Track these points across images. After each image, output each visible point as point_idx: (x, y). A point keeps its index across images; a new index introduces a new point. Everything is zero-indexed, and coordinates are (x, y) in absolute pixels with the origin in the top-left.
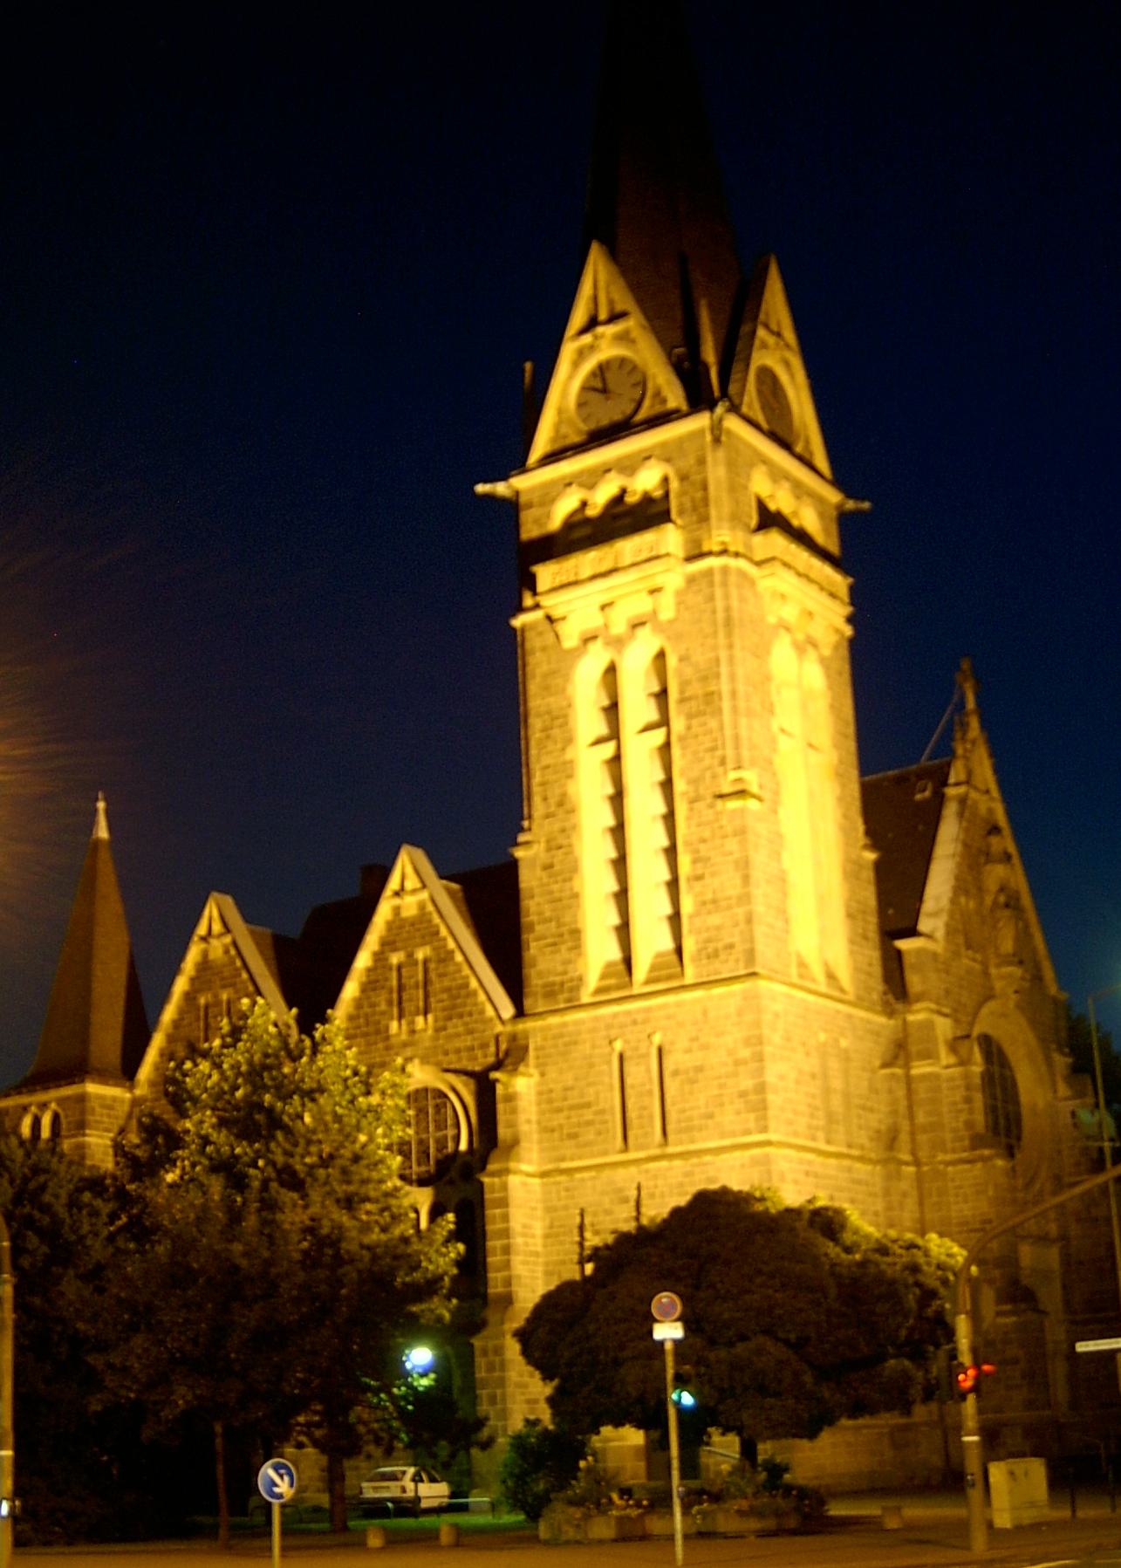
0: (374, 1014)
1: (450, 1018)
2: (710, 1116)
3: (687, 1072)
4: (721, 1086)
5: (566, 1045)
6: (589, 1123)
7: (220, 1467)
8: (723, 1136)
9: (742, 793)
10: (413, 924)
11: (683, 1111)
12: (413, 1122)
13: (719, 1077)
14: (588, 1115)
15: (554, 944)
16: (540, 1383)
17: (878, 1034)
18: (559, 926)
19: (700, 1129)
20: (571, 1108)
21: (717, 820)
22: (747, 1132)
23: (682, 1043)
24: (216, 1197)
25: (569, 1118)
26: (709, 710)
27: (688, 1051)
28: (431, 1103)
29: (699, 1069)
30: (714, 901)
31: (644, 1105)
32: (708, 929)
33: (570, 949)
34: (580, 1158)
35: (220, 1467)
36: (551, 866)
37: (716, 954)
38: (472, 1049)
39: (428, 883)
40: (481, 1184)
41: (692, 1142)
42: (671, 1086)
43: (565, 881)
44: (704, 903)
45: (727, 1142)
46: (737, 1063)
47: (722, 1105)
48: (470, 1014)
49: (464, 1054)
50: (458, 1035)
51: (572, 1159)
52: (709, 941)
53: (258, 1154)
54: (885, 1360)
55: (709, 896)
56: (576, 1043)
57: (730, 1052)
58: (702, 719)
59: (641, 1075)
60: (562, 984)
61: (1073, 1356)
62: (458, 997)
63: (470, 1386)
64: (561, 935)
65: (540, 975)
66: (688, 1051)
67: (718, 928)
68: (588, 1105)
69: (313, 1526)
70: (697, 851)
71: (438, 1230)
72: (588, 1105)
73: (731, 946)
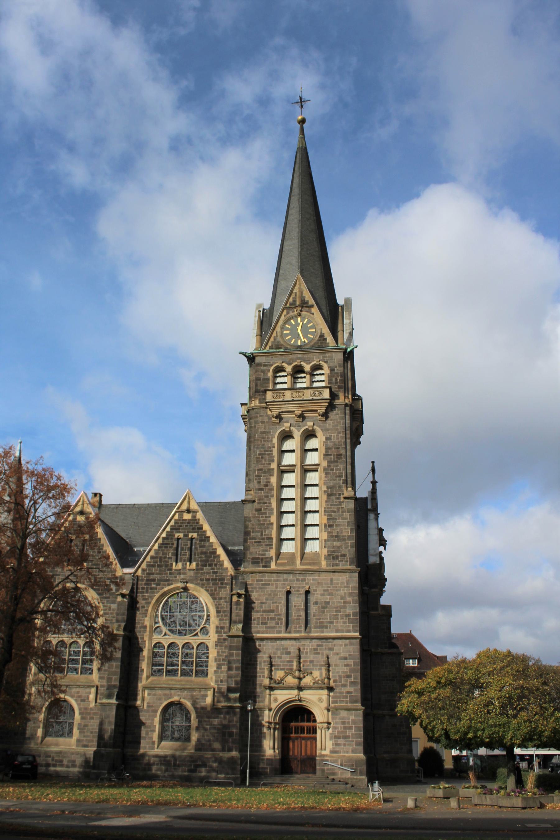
0: (165, 558)
1: (205, 566)
2: (331, 623)
3: (322, 603)
4: (337, 611)
5: (263, 584)
6: (272, 619)
7: (248, 770)
8: (337, 631)
9: (467, 808)
10: (189, 523)
11: (319, 619)
12: (23, 472)
13: (337, 607)
14: (272, 615)
15: (260, 542)
16: (465, 656)
17: (33, 707)
18: (262, 535)
19: (326, 627)
20: (264, 611)
21: (341, 505)
22: (349, 631)
23: (320, 590)
24: (32, 664)
25: (262, 615)
26: (79, 702)
27: (322, 595)
28: (198, 614)
29: (328, 603)
30: (337, 536)
31: (297, 611)
32: (334, 547)
33: (266, 545)
34: (267, 633)
35: (248, 770)
36: (260, 510)
37: (337, 557)
38: (216, 580)
39: (376, 532)
40: (365, 753)
41: (323, 632)
42: (313, 609)
43: (266, 517)
44: (332, 536)
45: (339, 634)
46: (345, 602)
47: (337, 619)
48: (216, 565)
49: (211, 582)
50: (208, 573)
51: (263, 633)
52: (334, 551)
53: (473, 709)
54: (519, 767)
55: (335, 534)
56: (268, 584)
57: (342, 598)
58: (336, 464)
59: (297, 600)
60: (262, 559)
61: (312, 322)
62: (210, 557)
63: (262, 513)
64: (263, 539)
65: (251, 553)
66: (322, 595)
67: (339, 547)
68: (272, 611)
69: (311, 829)
70: (331, 515)
71: (66, 635)
72: (272, 611)
73: (344, 555)
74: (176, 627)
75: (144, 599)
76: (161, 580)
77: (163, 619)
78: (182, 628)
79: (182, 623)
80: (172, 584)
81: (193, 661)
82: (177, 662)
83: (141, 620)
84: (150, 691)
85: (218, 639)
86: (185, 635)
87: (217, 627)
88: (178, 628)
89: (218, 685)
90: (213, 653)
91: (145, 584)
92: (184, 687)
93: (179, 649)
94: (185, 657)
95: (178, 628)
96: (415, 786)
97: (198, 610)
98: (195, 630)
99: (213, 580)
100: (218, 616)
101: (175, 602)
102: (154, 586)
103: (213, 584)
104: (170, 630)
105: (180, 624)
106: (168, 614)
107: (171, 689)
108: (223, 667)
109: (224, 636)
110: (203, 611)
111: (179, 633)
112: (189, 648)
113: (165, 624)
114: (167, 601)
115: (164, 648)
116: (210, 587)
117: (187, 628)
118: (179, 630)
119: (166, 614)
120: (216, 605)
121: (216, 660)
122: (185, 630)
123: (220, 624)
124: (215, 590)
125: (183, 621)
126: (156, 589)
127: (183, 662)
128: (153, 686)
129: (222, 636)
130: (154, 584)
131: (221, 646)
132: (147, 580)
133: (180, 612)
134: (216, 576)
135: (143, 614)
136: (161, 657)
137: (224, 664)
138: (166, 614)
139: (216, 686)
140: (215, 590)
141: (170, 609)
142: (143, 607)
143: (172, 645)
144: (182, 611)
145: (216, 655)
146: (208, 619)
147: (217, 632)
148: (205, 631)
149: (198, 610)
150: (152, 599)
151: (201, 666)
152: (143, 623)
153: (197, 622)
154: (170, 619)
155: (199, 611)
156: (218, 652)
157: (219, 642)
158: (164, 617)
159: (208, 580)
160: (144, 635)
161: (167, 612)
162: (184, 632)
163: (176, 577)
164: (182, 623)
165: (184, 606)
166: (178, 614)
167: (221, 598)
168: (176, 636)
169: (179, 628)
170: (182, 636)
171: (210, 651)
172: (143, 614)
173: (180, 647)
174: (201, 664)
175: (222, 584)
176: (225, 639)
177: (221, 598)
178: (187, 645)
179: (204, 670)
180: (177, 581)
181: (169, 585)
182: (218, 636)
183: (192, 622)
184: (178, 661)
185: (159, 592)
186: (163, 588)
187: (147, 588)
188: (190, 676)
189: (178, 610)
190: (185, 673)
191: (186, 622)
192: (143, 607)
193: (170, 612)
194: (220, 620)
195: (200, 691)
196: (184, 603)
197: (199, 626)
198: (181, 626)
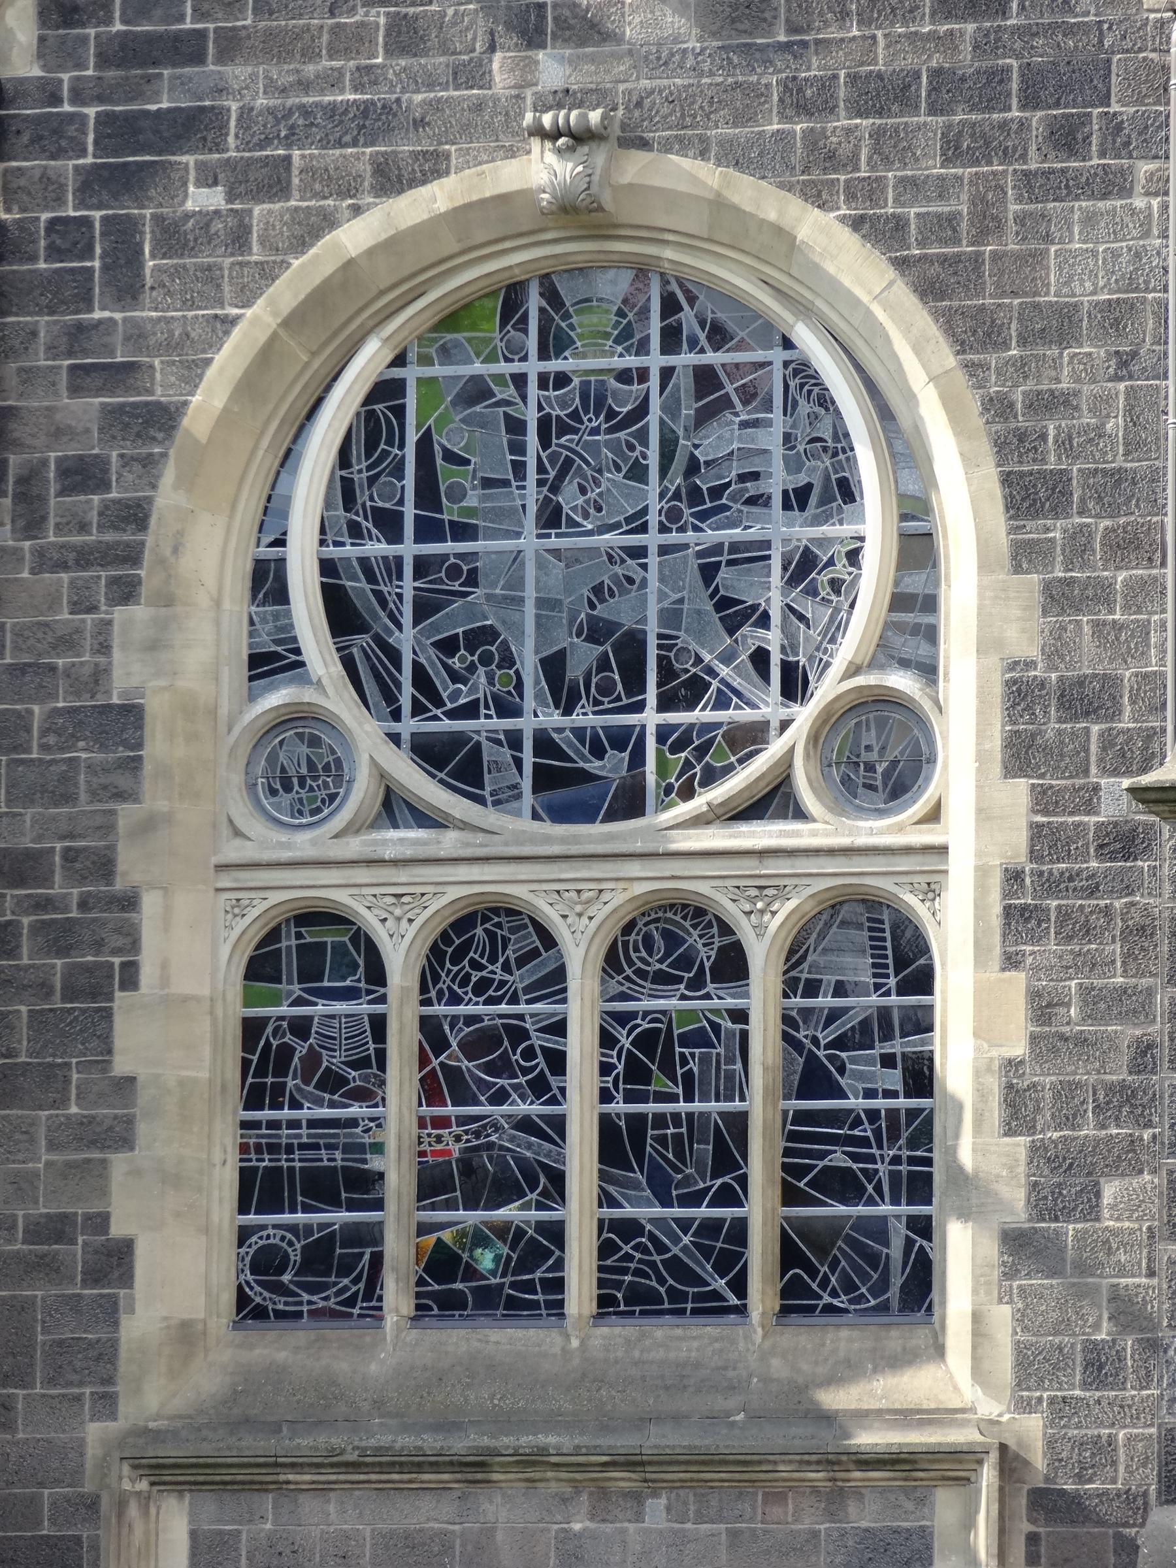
28: (785, 532)
38: (988, 89)
74: (507, 709)
75: (83, 379)
76: (295, 126)
77: (342, 616)
78: (585, 718)
79: (582, 658)
80: (433, 167)
81: (739, 1123)
82: (531, 1149)
83: (68, 642)
84: (216, 1514)
85: (1043, 840)
86: (630, 803)
87: (1021, 694)
88: (539, 716)
89: (1061, 1408)
90: (973, 1026)
91: (94, 184)
92: (625, 1442)
93: (554, 983)
94: (636, 1073)
95: (539, 716)
96: (255, 351)
97: (777, 481)
98: (749, 738)
99: (946, 88)
100: (1025, 555)
101: (476, 392)
102: (202, 199)
103: (953, 151)
104: (430, 753)
105: (554, 666)
106: (409, 549)
107: (475, 1468)
108: (1110, 1191)
109: (1114, 797)
110: (847, 491)
111: (544, 779)
112: (680, 970)
113: (373, 677)
114: (385, 392)
115: (377, 974)
116: (911, 187)
117: (651, 718)
118: (544, 744)
119: (377, 548)
120: (998, 408)
121: (1018, 1108)
122: (620, 738)
123: (1054, 653)
124: (987, 223)
125: (596, 632)
126: (239, 238)
127: (617, 1145)
128: (255, 1445)
129: (1089, 800)
130: (208, 178)
131: (1076, 928)
132: (120, 132)
133: (551, 518)
134: (985, 45)
135: (85, 558)
136: (332, 1082)
137: (1127, 1159)
138: (377, 548)
139: (1032, 1429)
140: (987, 223)
141: (428, 493)
142: (83, 475)
143: (484, 943)
144: (569, 498)
145: (1019, 1049)
146: (914, 611)
147: (1021, 755)
148: (881, 756)
149: (777, 481)
150: (193, 373)
151: (845, 1186)
152: (100, 675)
153: (773, 640)
154: (423, 610)
155: (797, 499)
156: (1043, 1008)
157: (1050, 885)
158: (357, 586)
159: (883, 95)
160: (108, 828)
161: (389, 524)
162: (611, 766)
163: (473, 74)
164: (582, 658)
165: (595, 439)
166: (529, 541)
167: (1060, 325)
168: (519, 825)
169: (553, 719)
170: (585, 813)
171: (385, 1304)
172: (85, 558)
173: (402, 959)
174: (839, 1158)
175: (1067, 138)
176: (1124, 843)
177: (1060, 325)
178: (676, 942)
179: (878, 1229)
180: (502, 133)
181: (391, 180)
182: (1043, 800)
183: (708, 649)
184: (555, 1129)
185: (268, 273)
186: (310, 229)
187: (123, 233)
188: (712, 1307)
189: (531, 495)
190: (640, 1283)
191: (631, 650)
192: (83, 475)
193: (427, 530)
194: (1058, 598)
195: (835, 1499)
196: (594, 399)
197: (795, 685)
198: (564, 696)
